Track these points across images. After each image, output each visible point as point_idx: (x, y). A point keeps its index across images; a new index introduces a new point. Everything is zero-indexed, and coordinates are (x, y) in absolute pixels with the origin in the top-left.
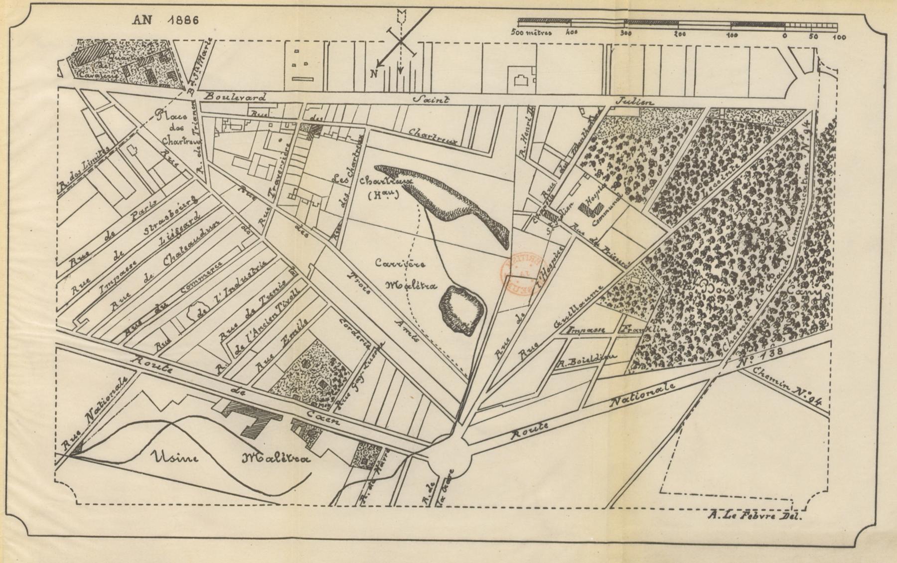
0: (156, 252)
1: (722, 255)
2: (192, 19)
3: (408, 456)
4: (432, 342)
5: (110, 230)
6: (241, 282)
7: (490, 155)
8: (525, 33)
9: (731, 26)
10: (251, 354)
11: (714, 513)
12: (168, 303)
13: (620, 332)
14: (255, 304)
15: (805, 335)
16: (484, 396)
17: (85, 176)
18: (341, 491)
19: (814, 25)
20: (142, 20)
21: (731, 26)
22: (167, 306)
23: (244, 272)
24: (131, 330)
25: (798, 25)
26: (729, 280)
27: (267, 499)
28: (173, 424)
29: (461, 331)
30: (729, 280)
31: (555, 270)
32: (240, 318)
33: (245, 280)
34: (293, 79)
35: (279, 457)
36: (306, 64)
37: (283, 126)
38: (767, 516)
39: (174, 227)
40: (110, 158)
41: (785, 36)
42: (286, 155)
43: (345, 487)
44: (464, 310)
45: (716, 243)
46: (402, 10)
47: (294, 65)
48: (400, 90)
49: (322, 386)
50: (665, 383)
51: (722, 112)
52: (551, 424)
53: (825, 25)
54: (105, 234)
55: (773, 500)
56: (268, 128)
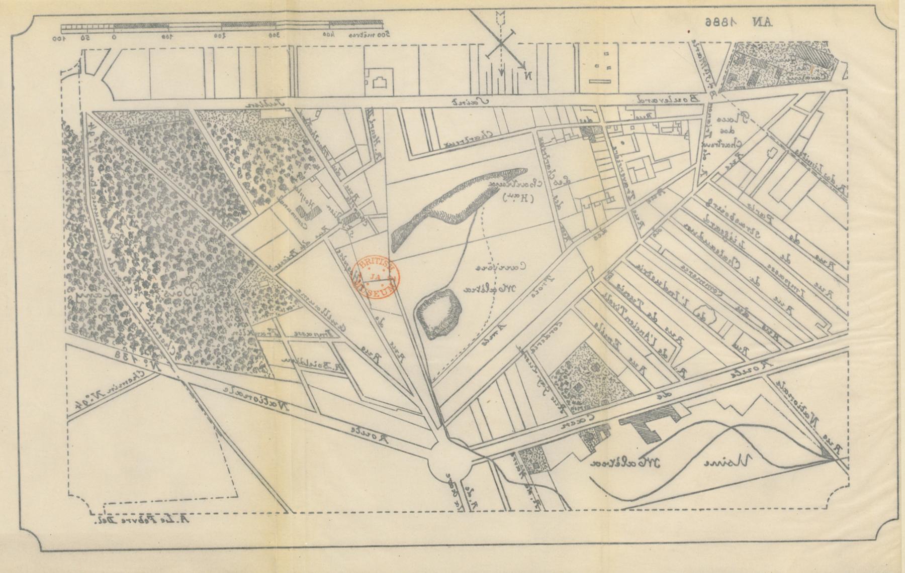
0: (760, 265)
1: (177, 258)
2: (713, 21)
3: (492, 460)
4: (469, 345)
5: (799, 237)
6: (662, 286)
7: (411, 158)
8: (376, 36)
9: (222, 27)
10: (646, 352)
11: (183, 518)
12: (750, 317)
13: (279, 336)
14: (662, 321)
15: (93, 339)
16: (416, 399)
17: (820, 179)
18: (560, 495)
19: (90, 27)
20: (763, 23)
21: (222, 27)
22: (747, 317)
23: (660, 276)
24: (773, 335)
25: (69, 27)
26: (169, 283)
27: (635, 505)
28: (730, 428)
29: (438, 335)
30: (169, 283)
31: (343, 269)
32: (648, 308)
33: (665, 289)
34: (608, 82)
35: (624, 462)
36: (597, 66)
37: (620, 129)
38: (129, 520)
39: (735, 234)
40: (798, 164)
41: (114, 38)
42: (616, 157)
43: (556, 491)
44: (436, 314)
45: (180, 245)
46: (500, 11)
47: (609, 68)
48: (495, 92)
49: (581, 392)
50: (233, 387)
51: (177, 114)
52: (348, 428)
53: (101, 26)
54: (794, 234)
55: (123, 502)
56: (632, 132)
